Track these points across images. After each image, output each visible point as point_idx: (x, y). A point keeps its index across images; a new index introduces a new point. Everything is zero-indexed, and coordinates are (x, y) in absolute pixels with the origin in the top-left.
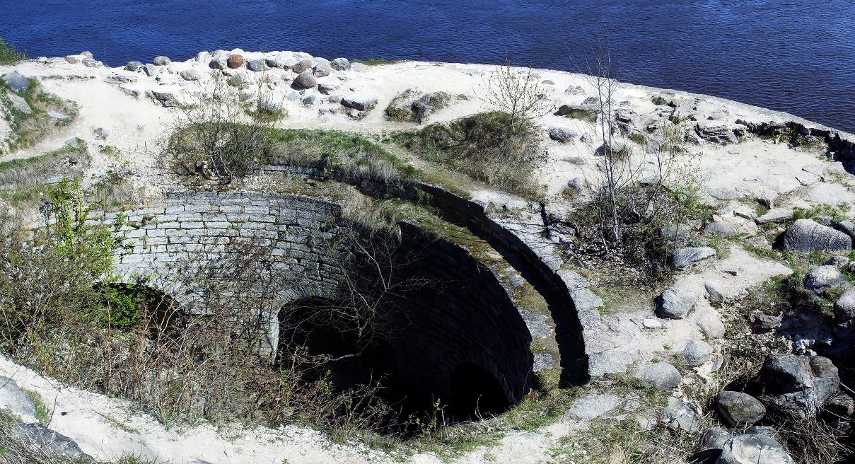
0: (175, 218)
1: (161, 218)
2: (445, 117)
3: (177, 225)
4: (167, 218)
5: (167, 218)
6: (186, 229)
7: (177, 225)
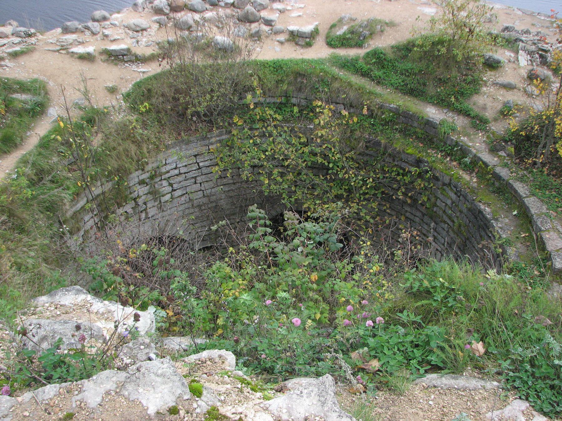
0: (174, 166)
1: (163, 170)
2: (384, 42)
3: (176, 172)
4: (168, 167)
5: (168, 167)
6: (185, 173)
7: (176, 172)
